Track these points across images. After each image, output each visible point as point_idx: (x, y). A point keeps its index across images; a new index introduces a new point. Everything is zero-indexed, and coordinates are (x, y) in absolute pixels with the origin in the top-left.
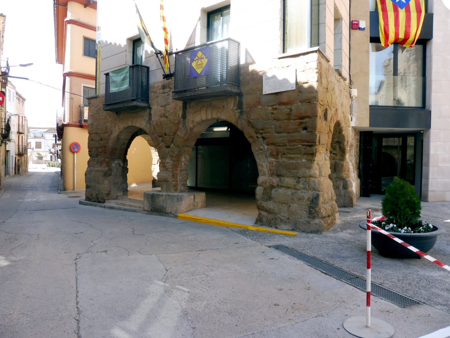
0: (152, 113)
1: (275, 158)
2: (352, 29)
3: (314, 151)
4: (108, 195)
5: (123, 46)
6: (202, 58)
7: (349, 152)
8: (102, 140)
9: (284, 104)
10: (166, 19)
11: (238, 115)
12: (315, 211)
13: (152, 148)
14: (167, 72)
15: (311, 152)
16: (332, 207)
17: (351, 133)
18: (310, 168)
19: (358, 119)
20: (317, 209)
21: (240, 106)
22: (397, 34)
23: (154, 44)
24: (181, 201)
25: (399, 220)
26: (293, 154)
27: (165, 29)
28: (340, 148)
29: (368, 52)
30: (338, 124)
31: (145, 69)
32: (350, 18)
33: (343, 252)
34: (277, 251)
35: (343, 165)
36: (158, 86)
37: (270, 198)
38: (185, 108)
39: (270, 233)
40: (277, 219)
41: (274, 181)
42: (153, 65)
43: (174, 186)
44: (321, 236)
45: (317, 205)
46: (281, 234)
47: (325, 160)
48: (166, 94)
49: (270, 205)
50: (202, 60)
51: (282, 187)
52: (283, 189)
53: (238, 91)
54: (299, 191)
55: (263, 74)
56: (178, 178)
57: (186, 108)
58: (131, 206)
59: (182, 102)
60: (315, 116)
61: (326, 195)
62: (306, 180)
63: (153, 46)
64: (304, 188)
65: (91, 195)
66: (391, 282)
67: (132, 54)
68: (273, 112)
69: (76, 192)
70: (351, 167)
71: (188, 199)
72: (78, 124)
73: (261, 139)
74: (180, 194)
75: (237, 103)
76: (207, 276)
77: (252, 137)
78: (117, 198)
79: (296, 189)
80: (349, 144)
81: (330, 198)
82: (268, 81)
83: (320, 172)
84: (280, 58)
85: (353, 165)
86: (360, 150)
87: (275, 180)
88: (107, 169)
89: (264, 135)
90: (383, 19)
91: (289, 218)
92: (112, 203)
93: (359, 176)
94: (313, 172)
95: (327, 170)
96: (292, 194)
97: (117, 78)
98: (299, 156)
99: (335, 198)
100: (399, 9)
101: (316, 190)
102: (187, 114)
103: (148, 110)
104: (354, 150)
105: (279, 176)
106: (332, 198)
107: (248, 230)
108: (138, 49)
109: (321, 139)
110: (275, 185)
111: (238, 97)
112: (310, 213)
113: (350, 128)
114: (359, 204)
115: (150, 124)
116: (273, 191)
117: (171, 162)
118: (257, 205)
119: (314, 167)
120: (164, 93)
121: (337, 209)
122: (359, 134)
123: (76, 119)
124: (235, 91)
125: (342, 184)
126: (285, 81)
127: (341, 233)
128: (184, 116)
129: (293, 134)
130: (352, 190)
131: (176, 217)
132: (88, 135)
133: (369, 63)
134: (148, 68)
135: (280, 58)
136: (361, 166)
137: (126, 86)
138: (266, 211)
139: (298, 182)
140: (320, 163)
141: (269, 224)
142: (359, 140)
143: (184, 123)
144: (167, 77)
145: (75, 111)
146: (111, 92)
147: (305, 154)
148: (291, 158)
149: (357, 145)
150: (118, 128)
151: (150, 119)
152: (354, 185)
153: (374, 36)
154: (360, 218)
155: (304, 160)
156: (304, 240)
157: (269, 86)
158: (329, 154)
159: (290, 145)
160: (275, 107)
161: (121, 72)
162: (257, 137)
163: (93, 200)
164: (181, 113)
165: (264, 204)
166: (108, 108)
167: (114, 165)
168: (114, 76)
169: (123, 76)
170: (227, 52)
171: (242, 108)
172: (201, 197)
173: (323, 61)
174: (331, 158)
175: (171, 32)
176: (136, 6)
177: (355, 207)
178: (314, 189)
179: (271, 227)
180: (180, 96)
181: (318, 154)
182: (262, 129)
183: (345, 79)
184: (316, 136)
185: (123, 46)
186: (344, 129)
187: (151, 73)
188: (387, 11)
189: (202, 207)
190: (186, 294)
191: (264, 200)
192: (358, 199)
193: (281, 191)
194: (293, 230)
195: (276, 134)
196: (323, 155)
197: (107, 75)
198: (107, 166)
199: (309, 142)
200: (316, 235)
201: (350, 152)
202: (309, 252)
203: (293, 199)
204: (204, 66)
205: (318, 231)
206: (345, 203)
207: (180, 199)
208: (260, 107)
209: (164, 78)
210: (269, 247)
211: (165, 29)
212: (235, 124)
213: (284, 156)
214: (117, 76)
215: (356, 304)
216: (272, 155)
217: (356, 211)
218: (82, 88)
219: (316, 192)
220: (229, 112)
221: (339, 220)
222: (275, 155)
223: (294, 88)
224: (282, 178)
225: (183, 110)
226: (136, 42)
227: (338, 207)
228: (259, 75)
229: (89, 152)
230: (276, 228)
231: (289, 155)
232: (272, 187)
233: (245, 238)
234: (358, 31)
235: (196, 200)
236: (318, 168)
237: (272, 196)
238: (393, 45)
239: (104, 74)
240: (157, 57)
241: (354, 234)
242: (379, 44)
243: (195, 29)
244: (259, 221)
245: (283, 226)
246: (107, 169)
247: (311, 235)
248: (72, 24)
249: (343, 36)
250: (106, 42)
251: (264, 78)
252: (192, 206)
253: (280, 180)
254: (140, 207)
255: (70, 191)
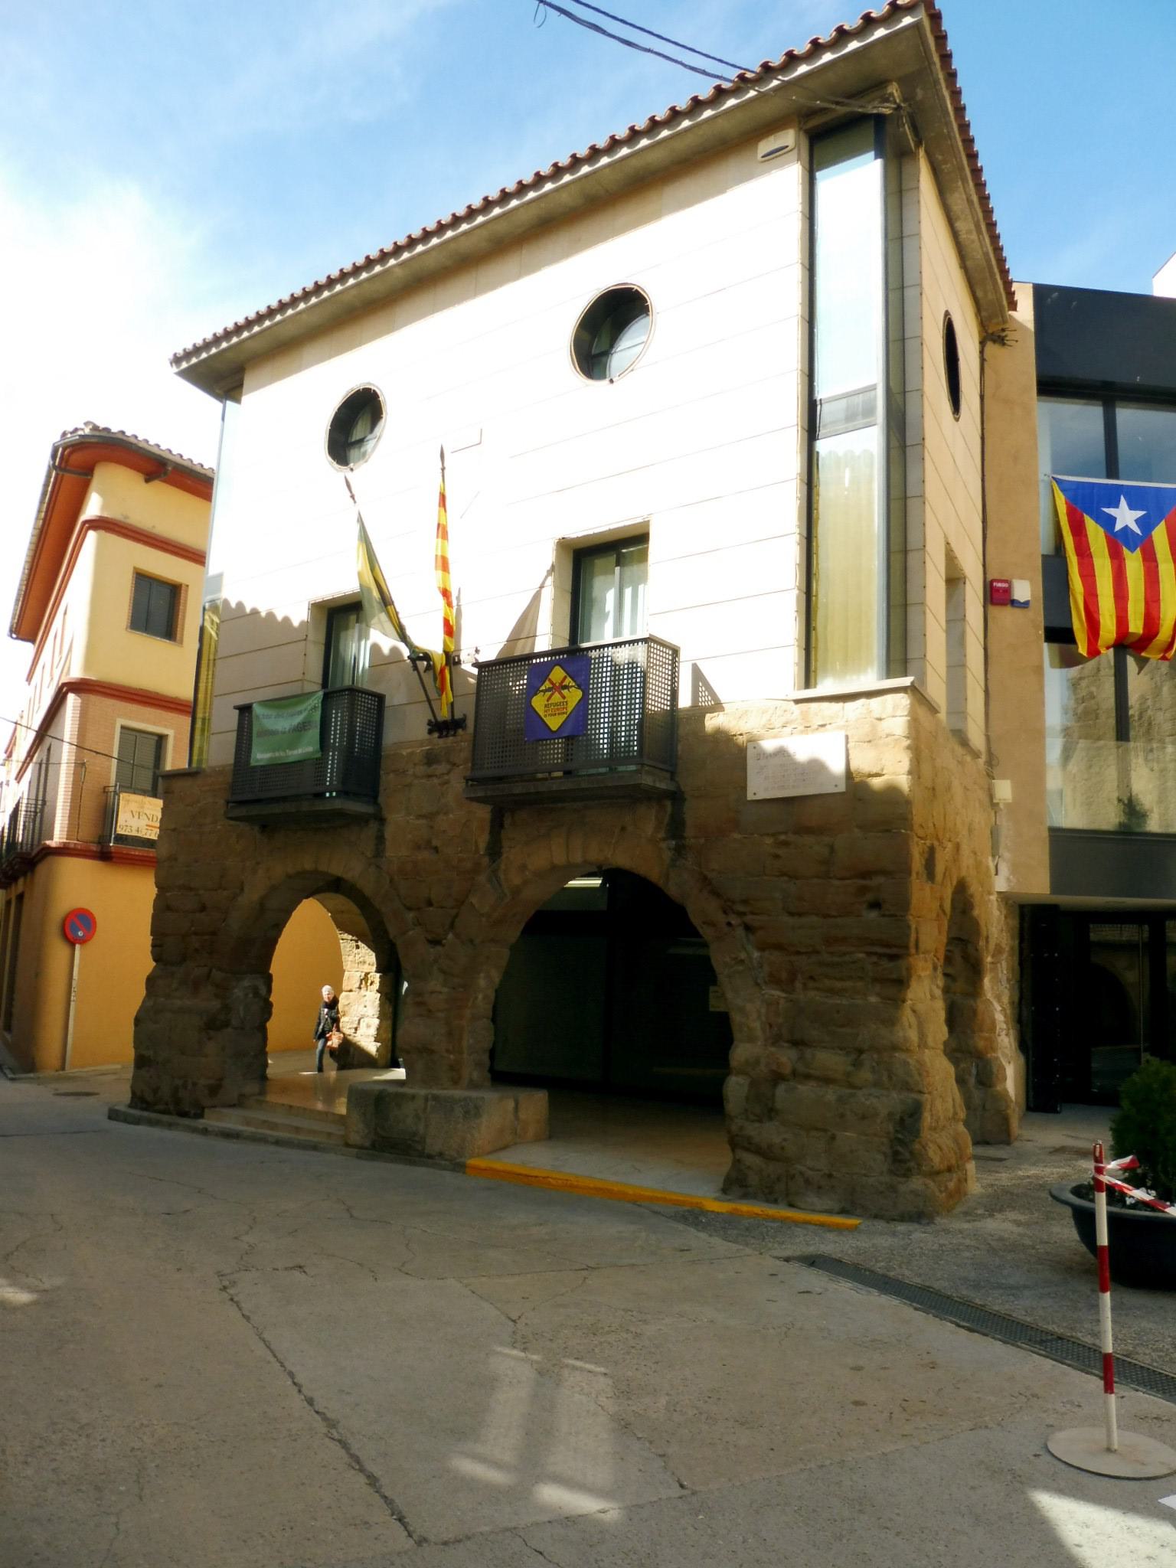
0: (387, 835)
1: (783, 991)
2: (993, 603)
3: (904, 973)
4: (214, 1090)
5: (296, 623)
6: (567, 687)
7: (992, 970)
8: (203, 908)
9: (808, 830)
10: (452, 566)
11: (668, 855)
12: (911, 1153)
13: (346, 936)
14: (444, 714)
15: (894, 976)
16: (956, 1141)
17: (996, 913)
18: (891, 1022)
19: (1015, 869)
20: (917, 1146)
21: (676, 828)
22: (1122, 620)
23: (409, 632)
24: (478, 1115)
25: (1163, 1177)
26: (841, 979)
27: (446, 593)
28: (966, 958)
29: (1039, 670)
30: (961, 888)
31: (372, 703)
32: (985, 573)
33: (1005, 1272)
34: (813, 1271)
35: (975, 1012)
36: (412, 753)
37: (771, 1113)
38: (497, 825)
39: (774, 1219)
40: (793, 1177)
41: (784, 1059)
42: (398, 693)
43: (452, 1068)
44: (929, 1229)
45: (916, 1133)
46: (808, 1223)
47: (933, 997)
48: (436, 781)
49: (770, 1133)
50: (565, 692)
51: (807, 1077)
52: (813, 1083)
53: (672, 787)
54: (860, 1093)
55: (749, 741)
56: (465, 1044)
57: (502, 826)
58: (297, 1130)
59: (489, 808)
60: (904, 869)
61: (938, 1103)
62: (881, 1058)
63: (403, 637)
64: (877, 1084)
65: (156, 1091)
66: (1153, 1350)
67: (323, 647)
68: (780, 852)
69: (69, 1079)
70: (1000, 1017)
71: (504, 1110)
72: (94, 848)
73: (740, 932)
74: (474, 1094)
75: (666, 820)
76: (637, 1335)
77: (711, 924)
78: (240, 1103)
79: (852, 1086)
80: (992, 947)
81: (951, 1115)
82: (762, 762)
83: (922, 1036)
84: (797, 702)
85: (1004, 1010)
86: (1021, 964)
87: (787, 1057)
88: (215, 1004)
89: (749, 918)
90: (1082, 576)
91: (830, 1176)
92: (231, 1120)
93: (1022, 1045)
94: (901, 1034)
95: (939, 1031)
96: (841, 1100)
97: (267, 720)
98: (860, 984)
99: (962, 1115)
100: (1126, 551)
101: (910, 1090)
102: (506, 844)
103: (373, 826)
104: (1004, 964)
105: (796, 1043)
106: (955, 1113)
107: (704, 1213)
108: (343, 635)
109: (922, 938)
110: (787, 1071)
111: (668, 804)
112: (896, 1158)
113: (993, 898)
114: (1026, 1133)
115: (378, 867)
116: (781, 1088)
117: (445, 990)
118: (729, 1132)
119: (904, 1019)
120: (429, 776)
121: (971, 1150)
122: (1017, 912)
123: (88, 832)
124: (662, 786)
125: (974, 1071)
126: (816, 767)
127: (989, 1220)
128: (495, 851)
129: (839, 920)
130: (1006, 1090)
131: (459, 1167)
132: (153, 891)
133: (1043, 703)
134: (380, 699)
135: (797, 702)
136: (1025, 1013)
137: (307, 747)
138: (759, 1151)
139: (857, 1064)
140: (919, 1007)
141: (769, 1195)
142: (1017, 931)
143: (495, 872)
144: (440, 728)
145: (90, 804)
146: (253, 763)
147: (875, 980)
148: (832, 992)
149: (1012, 948)
150: (262, 872)
151: (379, 852)
152: (1011, 1078)
153: (1057, 623)
154: (1037, 1177)
155: (873, 999)
156: (884, 1242)
157: (766, 778)
158: (941, 982)
159: (832, 953)
160: (783, 837)
161: (297, 704)
162: (729, 924)
163: (161, 1107)
164: (483, 840)
165: (752, 1130)
166: (242, 811)
167: (238, 993)
168: (268, 717)
169: (298, 720)
170: (645, 676)
171: (682, 837)
172: (535, 1104)
173: (922, 712)
174: (946, 991)
175: (458, 598)
176: (360, 520)
177: (1017, 1144)
178: (907, 1087)
179: (775, 1201)
180: (489, 793)
181: (914, 984)
182: (745, 902)
183: (976, 755)
184: (909, 927)
185: (296, 623)
186: (976, 900)
187: (388, 714)
188: (1090, 556)
189: (537, 1139)
190: (602, 1379)
191: (752, 1117)
192: (1022, 1118)
193: (806, 1090)
194: (843, 1212)
195: (791, 921)
196: (926, 983)
197: (245, 710)
198: (217, 996)
199: (888, 946)
200: (917, 1226)
201: (994, 970)
202: (907, 1273)
203: (842, 1116)
204: (570, 710)
205: (920, 1216)
206: (990, 1132)
207: (473, 1111)
208: (737, 836)
209: (430, 732)
210: (787, 1260)
211: (446, 593)
212: (661, 883)
213: (811, 984)
214: (278, 716)
215: (1072, 1403)
216: (774, 980)
217: (1022, 1158)
218: (118, 730)
219: (914, 1096)
220: (640, 848)
221: (977, 1183)
222: (786, 981)
223: (842, 788)
224: (808, 1053)
225: (491, 832)
226: (339, 615)
227: (976, 1143)
228: (737, 745)
229: (154, 946)
230: (791, 1205)
231: (827, 983)
232: (777, 1078)
233: (703, 1235)
234: (1009, 609)
235: (522, 1116)
236: (913, 1020)
237: (779, 1105)
238: (1112, 650)
239: (236, 708)
240: (415, 668)
241: (1027, 1225)
242: (1072, 646)
243: (537, 598)
244: (735, 1184)
245: (812, 1199)
246: (215, 1004)
247: (902, 1228)
248: (102, 532)
249: (968, 630)
250: (240, 605)
251: (750, 753)
252: (506, 1129)
253: (801, 1058)
254: (329, 1135)
255: (52, 1073)
